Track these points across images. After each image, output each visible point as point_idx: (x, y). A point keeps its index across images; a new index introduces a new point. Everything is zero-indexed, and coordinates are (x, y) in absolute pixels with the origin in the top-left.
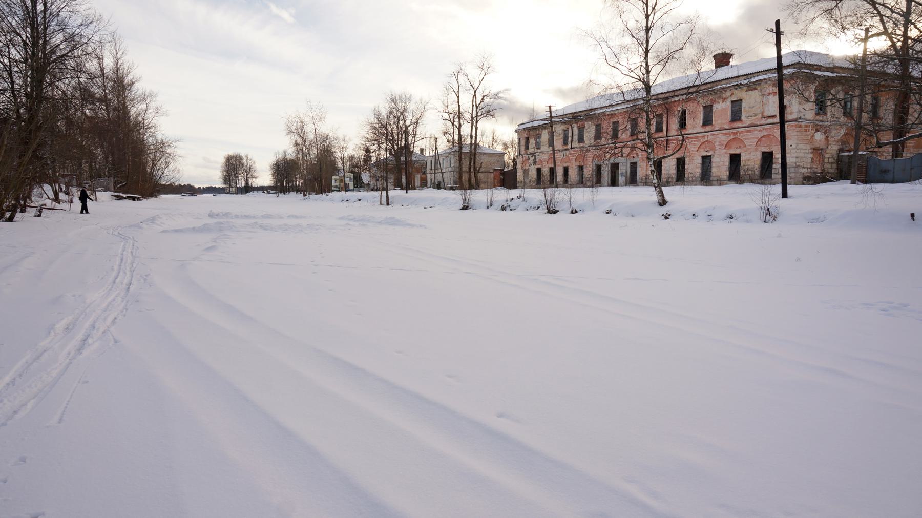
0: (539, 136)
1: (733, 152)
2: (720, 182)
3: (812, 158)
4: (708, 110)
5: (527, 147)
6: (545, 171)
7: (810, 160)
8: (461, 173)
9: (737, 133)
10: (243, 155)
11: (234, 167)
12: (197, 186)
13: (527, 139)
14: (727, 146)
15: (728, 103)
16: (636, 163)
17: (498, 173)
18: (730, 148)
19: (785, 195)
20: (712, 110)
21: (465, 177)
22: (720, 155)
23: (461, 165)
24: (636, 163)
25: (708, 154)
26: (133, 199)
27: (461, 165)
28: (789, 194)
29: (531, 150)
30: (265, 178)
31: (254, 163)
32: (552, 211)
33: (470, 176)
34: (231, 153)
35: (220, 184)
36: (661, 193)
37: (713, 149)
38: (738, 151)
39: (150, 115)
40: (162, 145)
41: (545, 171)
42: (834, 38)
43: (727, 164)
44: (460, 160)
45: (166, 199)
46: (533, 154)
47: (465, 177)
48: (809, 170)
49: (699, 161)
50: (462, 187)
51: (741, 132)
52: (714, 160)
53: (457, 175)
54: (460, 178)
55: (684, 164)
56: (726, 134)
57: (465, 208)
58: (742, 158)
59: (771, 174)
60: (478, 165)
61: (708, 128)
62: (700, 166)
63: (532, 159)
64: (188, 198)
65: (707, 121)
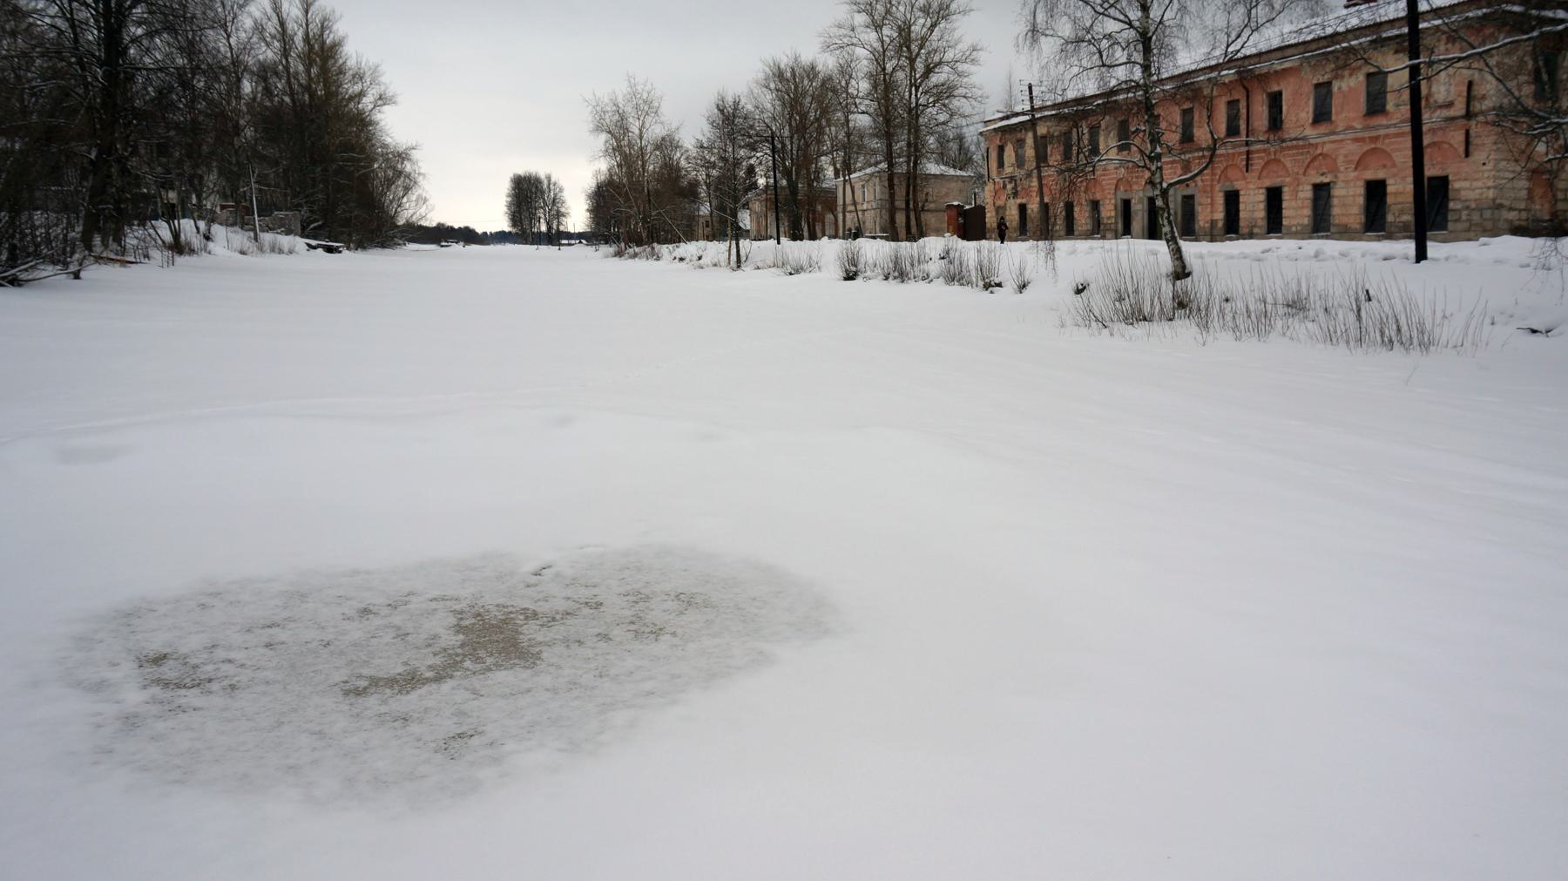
0: (1020, 143)
1: (1370, 175)
2: (1345, 234)
3: (1530, 191)
4: (1323, 93)
5: (1001, 164)
6: (1034, 207)
7: (1524, 194)
8: (892, 212)
9: (1377, 138)
10: (542, 176)
11: (529, 197)
12: (479, 231)
13: (1001, 149)
14: (1359, 164)
15: (1361, 77)
16: (1191, 197)
17: (954, 213)
18: (1366, 168)
19: (1421, 255)
20: (1330, 92)
21: (900, 218)
22: (1346, 182)
23: (892, 196)
24: (1191, 197)
25: (1326, 180)
26: (330, 250)
27: (892, 196)
28: (1429, 254)
29: (1008, 170)
30: (577, 218)
31: (561, 190)
32: (902, 276)
33: (908, 218)
34: (521, 171)
35: (504, 225)
36: (1177, 254)
37: (1334, 170)
38: (1380, 175)
39: (367, 102)
40: (402, 156)
41: (1034, 207)
42: (1023, 27)
43: (1361, 200)
44: (891, 186)
45: (413, 256)
46: (1012, 179)
47: (900, 218)
48: (1524, 215)
49: (1307, 193)
50: (894, 237)
51: (1387, 136)
52: (1337, 192)
53: (886, 217)
54: (892, 220)
55: (1280, 201)
56: (1356, 140)
57: (850, 277)
58: (1390, 189)
59: (1446, 221)
60: (921, 197)
61: (1323, 129)
62: (1309, 203)
63: (1009, 186)
64: (457, 248)
65: (1322, 115)
